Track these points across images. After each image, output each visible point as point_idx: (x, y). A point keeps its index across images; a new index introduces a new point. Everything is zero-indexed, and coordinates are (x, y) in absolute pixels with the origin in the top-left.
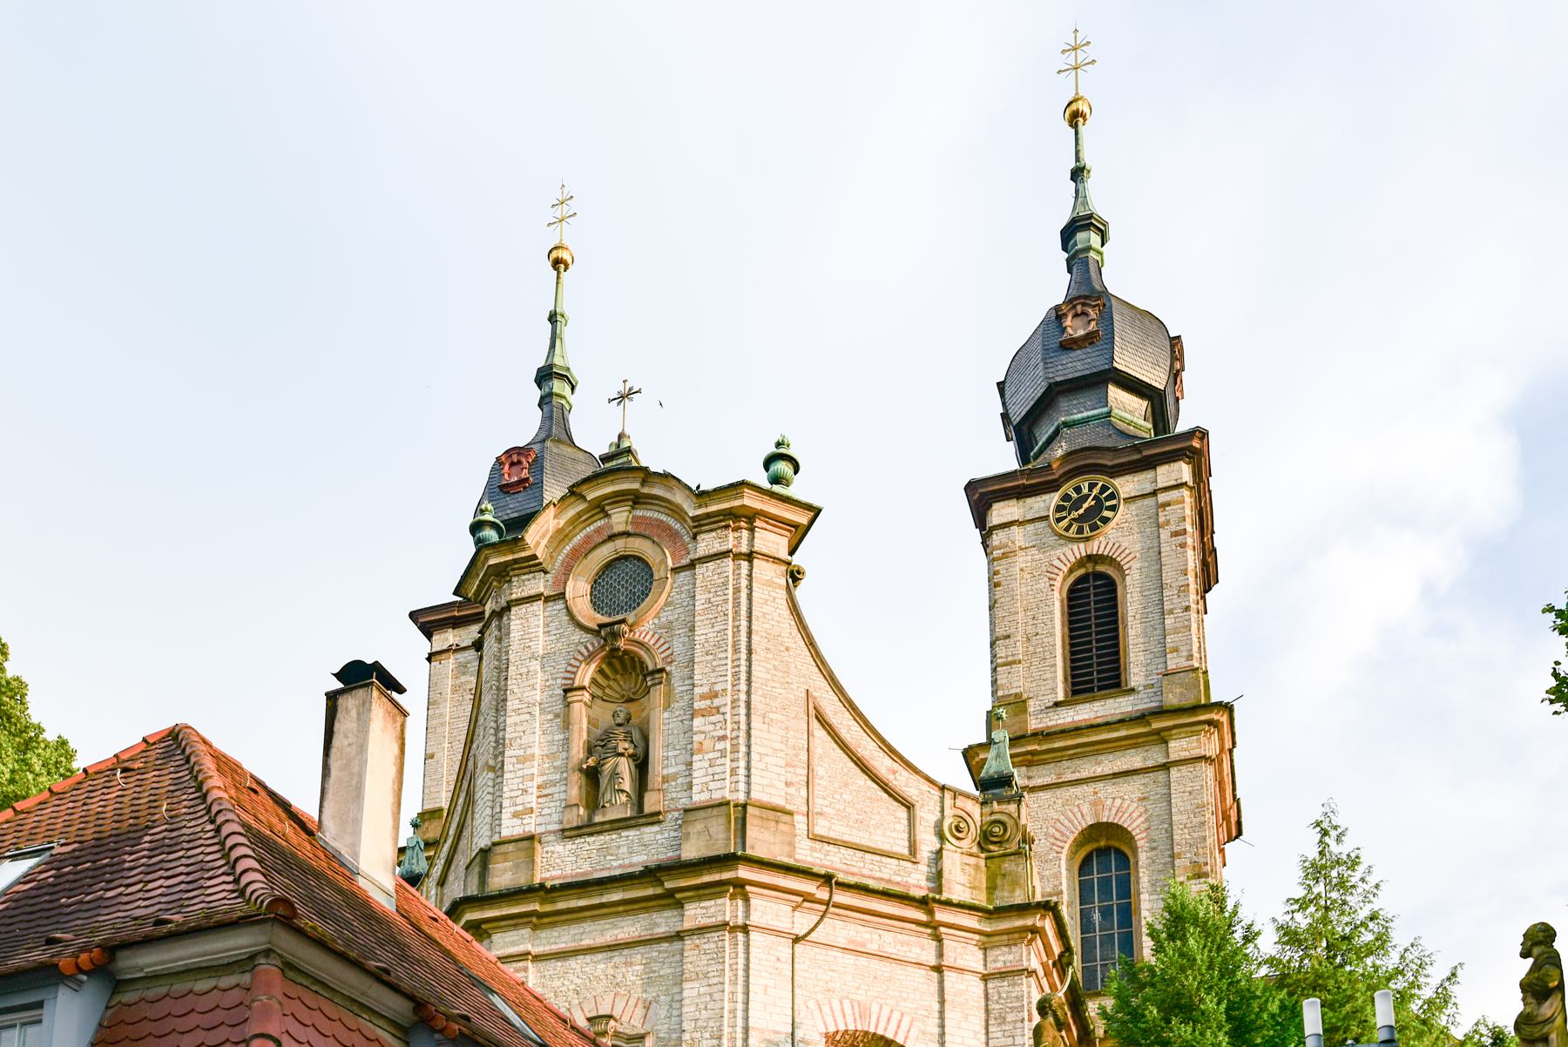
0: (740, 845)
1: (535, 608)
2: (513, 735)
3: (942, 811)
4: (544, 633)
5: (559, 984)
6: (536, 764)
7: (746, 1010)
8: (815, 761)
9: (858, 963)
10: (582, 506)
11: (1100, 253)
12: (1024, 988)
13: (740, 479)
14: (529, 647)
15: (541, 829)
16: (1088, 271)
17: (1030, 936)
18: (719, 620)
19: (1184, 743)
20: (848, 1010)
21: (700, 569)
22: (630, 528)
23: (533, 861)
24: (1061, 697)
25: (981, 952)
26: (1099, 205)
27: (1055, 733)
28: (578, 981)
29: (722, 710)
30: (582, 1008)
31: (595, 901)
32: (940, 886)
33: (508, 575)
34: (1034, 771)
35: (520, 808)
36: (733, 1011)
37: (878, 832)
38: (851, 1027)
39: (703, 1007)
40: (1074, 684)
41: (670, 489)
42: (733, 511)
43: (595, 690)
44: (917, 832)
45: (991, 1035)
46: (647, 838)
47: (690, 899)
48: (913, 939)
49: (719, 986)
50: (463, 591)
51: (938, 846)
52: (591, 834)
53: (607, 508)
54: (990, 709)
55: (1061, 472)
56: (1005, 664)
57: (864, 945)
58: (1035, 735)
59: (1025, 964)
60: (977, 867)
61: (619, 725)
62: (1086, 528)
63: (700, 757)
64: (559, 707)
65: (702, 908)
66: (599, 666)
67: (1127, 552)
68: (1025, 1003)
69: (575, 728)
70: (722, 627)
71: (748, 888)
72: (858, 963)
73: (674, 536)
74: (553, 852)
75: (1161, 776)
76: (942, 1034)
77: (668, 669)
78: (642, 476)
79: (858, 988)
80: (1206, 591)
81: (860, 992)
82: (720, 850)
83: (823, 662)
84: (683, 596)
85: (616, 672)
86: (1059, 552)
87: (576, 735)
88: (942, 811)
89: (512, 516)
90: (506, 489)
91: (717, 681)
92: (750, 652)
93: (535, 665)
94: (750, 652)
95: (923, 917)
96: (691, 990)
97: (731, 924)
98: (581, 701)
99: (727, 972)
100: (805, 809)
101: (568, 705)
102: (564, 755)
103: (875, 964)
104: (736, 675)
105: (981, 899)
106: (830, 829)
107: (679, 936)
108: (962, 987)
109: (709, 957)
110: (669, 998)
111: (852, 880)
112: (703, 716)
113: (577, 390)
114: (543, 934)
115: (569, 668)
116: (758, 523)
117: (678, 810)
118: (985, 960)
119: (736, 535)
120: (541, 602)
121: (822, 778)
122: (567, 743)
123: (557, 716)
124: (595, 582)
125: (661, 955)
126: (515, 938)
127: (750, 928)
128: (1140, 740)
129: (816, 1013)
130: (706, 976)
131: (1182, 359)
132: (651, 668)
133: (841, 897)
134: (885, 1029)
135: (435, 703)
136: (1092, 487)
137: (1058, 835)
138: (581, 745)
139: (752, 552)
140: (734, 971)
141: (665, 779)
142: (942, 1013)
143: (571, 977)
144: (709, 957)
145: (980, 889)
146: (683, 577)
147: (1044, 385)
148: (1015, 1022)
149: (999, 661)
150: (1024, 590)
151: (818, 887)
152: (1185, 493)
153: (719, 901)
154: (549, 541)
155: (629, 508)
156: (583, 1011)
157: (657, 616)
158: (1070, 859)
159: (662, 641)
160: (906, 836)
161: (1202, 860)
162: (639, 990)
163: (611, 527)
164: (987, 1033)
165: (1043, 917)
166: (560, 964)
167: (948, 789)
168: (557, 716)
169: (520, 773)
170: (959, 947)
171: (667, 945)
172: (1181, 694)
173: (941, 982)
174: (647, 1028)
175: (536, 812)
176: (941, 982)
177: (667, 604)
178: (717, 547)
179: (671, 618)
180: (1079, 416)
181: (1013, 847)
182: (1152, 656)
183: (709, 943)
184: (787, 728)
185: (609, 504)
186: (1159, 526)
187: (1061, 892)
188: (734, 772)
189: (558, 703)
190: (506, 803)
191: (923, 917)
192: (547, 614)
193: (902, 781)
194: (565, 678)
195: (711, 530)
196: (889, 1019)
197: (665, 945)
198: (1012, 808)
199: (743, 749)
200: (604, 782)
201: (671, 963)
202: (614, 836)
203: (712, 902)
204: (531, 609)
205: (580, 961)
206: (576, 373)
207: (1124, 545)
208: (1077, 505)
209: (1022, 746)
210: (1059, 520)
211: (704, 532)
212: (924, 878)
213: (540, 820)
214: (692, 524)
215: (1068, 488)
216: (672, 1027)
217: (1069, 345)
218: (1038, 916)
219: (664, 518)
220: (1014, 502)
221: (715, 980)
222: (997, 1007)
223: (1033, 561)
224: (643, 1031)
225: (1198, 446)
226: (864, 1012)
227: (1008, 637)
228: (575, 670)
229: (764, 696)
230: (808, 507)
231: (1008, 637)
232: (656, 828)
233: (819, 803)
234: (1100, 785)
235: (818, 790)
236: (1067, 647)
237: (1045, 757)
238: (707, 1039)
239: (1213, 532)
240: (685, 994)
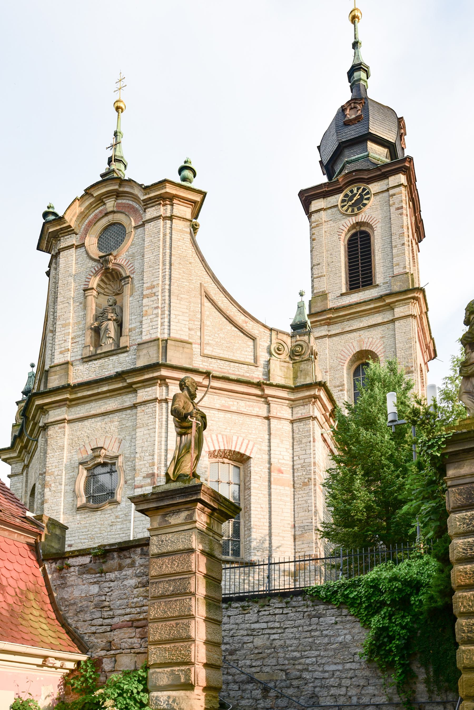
0: (164, 360)
1: (71, 252)
2: (60, 314)
3: (271, 341)
6: (71, 327)
7: (167, 441)
8: (205, 318)
9: (226, 416)
10: (92, 200)
11: (366, 82)
12: (311, 426)
13: (163, 179)
15: (73, 359)
16: (360, 90)
17: (313, 400)
19: (401, 309)
20: (220, 439)
21: (147, 226)
22: (115, 209)
23: (68, 374)
24: (344, 291)
25: (290, 409)
26: (365, 59)
27: (340, 308)
28: (89, 432)
29: (156, 294)
31: (95, 391)
32: (269, 377)
33: (59, 237)
34: (331, 327)
35: (63, 349)
36: (160, 442)
37: (238, 352)
38: (222, 448)
40: (350, 285)
41: (132, 187)
42: (162, 195)
43: (99, 290)
44: (258, 352)
45: (295, 450)
46: (121, 359)
47: (140, 388)
48: (255, 404)
49: (153, 430)
51: (269, 358)
52: (96, 360)
53: (104, 200)
54: (311, 299)
55: (343, 183)
56: (317, 278)
57: (229, 407)
58: (330, 309)
59: (311, 414)
60: (288, 368)
61: (110, 306)
62: (356, 209)
63: (146, 318)
64: (82, 299)
66: (101, 278)
67: (375, 219)
68: (311, 433)
69: (89, 308)
71: (167, 380)
72: (226, 416)
73: (135, 211)
74: (78, 370)
75: (391, 326)
76: (270, 450)
77: (132, 276)
79: (226, 429)
80: (420, 242)
81: (227, 430)
82: (154, 361)
83: (209, 269)
84: (140, 240)
86: (343, 222)
87: (89, 312)
88: (271, 341)
92: (171, 265)
93: (71, 280)
94: (171, 265)
95: (259, 392)
96: (140, 433)
97: (159, 399)
98: (92, 295)
99: (157, 423)
100: (199, 341)
101: (85, 297)
102: (84, 322)
103: (235, 417)
104: (164, 276)
105: (291, 383)
106: (212, 351)
107: (135, 406)
108: (280, 427)
109: (148, 415)
110: (130, 437)
111: (221, 375)
113: (128, 167)
114: (73, 410)
115: (87, 280)
116: (175, 201)
118: (292, 413)
119: (165, 208)
121: (208, 326)
124: (100, 237)
126: (59, 412)
128: (381, 309)
131: (404, 127)
132: (124, 276)
133: (215, 384)
134: (240, 449)
136: (358, 189)
137: (342, 357)
138: (92, 316)
139: (172, 216)
140: (161, 422)
141: (130, 330)
142: (269, 440)
143: (85, 429)
145: (289, 378)
146: (140, 230)
147: (337, 143)
148: (306, 443)
149: (315, 276)
150: (326, 241)
151: (203, 379)
152: (402, 189)
153: (154, 388)
154: (77, 218)
157: (127, 251)
158: (349, 369)
159: (130, 263)
160: (252, 354)
161: (410, 365)
162: (117, 434)
163: (106, 209)
164: (293, 449)
165: (319, 390)
167: (274, 330)
168: (81, 303)
169: (63, 332)
170: (279, 407)
172: (400, 285)
173: (269, 425)
174: (120, 452)
175: (71, 351)
176: (269, 425)
178: (155, 214)
179: (134, 251)
180: (354, 157)
181: (306, 357)
182: (387, 268)
183: (148, 409)
184: (190, 302)
187: (344, 385)
188: (162, 324)
190: (57, 347)
191: (259, 392)
193: (250, 326)
195: (153, 206)
196: (242, 443)
197: (129, 411)
198: (306, 338)
199: (167, 312)
200: (102, 333)
202: (106, 360)
203: (150, 389)
206: (126, 159)
207: (373, 216)
208: (351, 199)
209: (325, 315)
210: (343, 207)
212: (261, 374)
213: (73, 354)
214: (143, 204)
215: (347, 191)
217: (347, 123)
218: (317, 390)
219: (131, 203)
220: (322, 199)
221: (151, 427)
222: (298, 436)
223: (331, 227)
224: (118, 454)
225: (408, 165)
227: (319, 264)
229: (178, 286)
230: (200, 192)
231: (319, 264)
232: (125, 354)
233: (207, 338)
234: (362, 332)
235: (206, 332)
236: (347, 267)
237: (336, 320)
239: (420, 211)
240: (137, 435)
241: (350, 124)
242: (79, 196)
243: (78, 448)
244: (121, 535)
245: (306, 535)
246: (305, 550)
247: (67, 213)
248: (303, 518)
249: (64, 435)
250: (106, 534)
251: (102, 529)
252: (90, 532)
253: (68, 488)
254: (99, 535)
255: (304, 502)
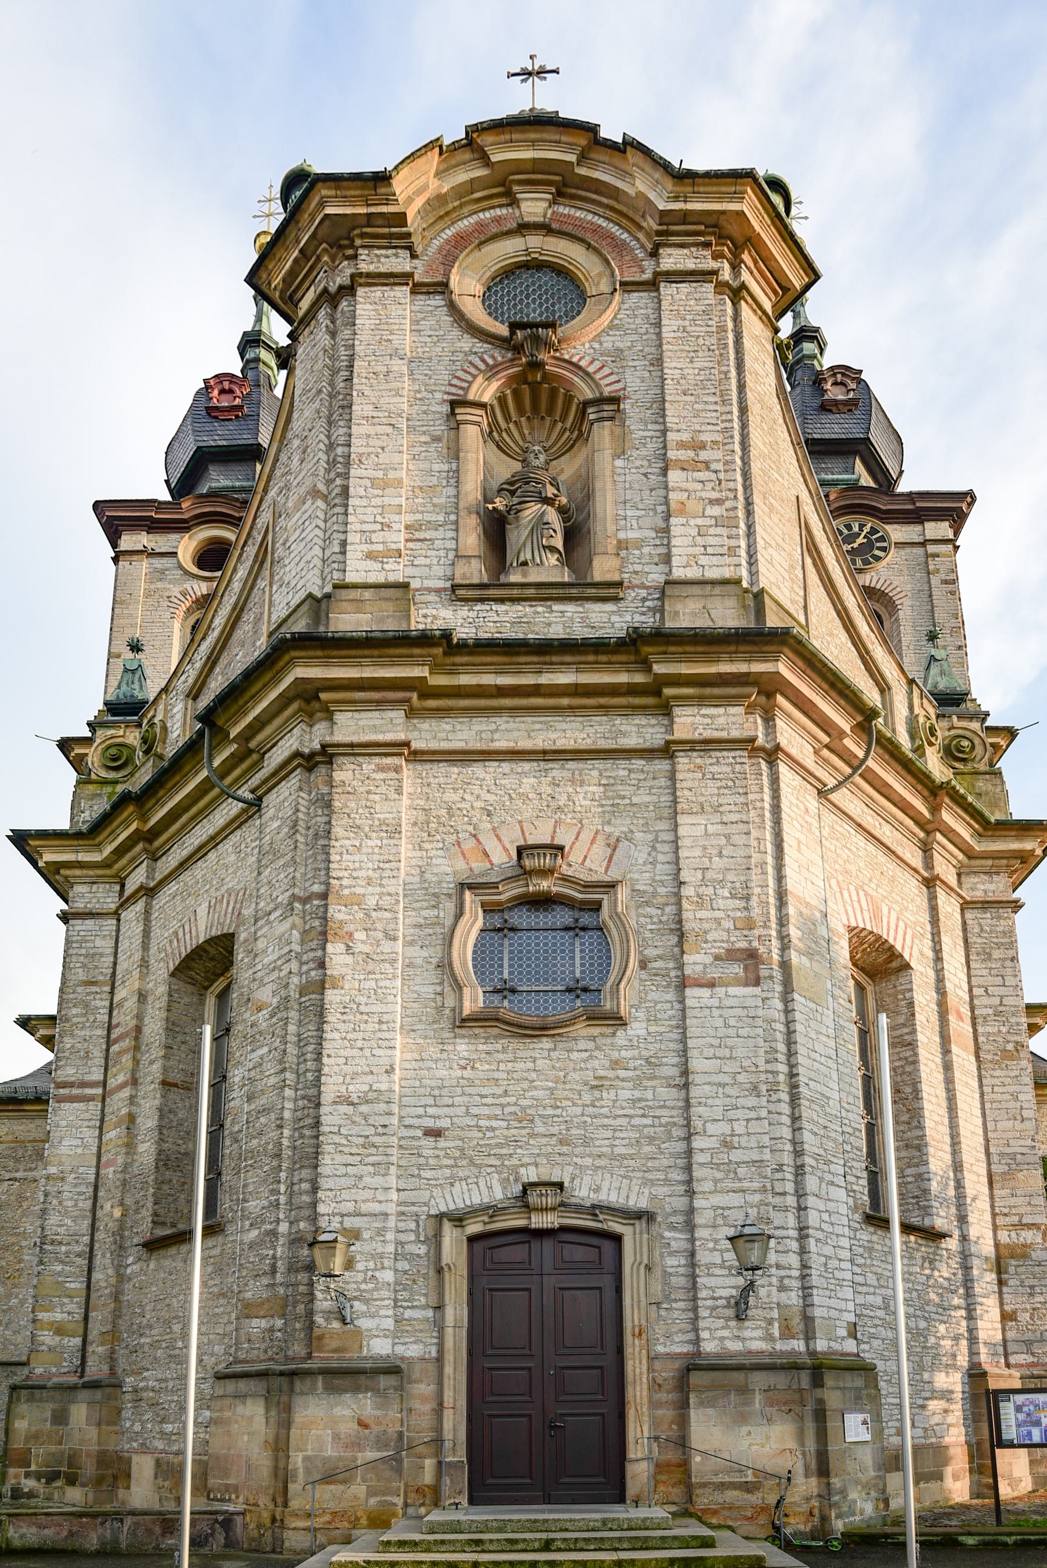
4: (411, 331)
5: (456, 797)
10: (481, 172)
14: (388, 340)
18: (700, 354)
28: (491, 798)
30: (497, 836)
33: (352, 246)
39: (715, 852)
47: (685, 700)
50: (264, 276)
52: (501, 600)
63: (683, 520)
64: (440, 428)
65: (703, 716)
70: (706, 364)
78: (583, 142)
84: (638, 321)
85: (521, 411)
89: (220, 443)
90: (212, 413)
91: (703, 428)
109: (719, 784)
110: (650, 837)
112: (683, 469)
117: (643, 586)
120: (407, 289)
122: (456, 477)
123: (437, 439)
125: (632, 776)
126: (378, 722)
127: (781, 755)
129: (838, 895)
130: (717, 809)
135: (122, 602)
136: (861, 527)
143: (476, 790)
144: (719, 784)
148: (1004, 960)
155: (550, 197)
156: (499, 839)
157: (597, 338)
166: (456, 770)
171: (643, 762)
177: (611, 326)
179: (620, 345)
185: (520, 183)
186: (929, 573)
189: (438, 423)
192: (414, 308)
194: (448, 393)
195: (682, 246)
197: (639, 763)
201: (651, 788)
202: (540, 609)
204: (392, 294)
205: (491, 770)
211: (671, 245)
216: (658, 878)
222: (979, 940)
226: (876, 915)
228: (465, 385)
232: (609, 607)
238: (723, 898)
241: (834, 409)
242: (447, 141)
243: (452, 838)
244: (636, 1121)
245: (1020, 1175)
246: (1022, 1210)
247: (405, 172)
248: (1010, 1135)
249: (400, 793)
250: (579, 1110)
251: (559, 1093)
252: (512, 1100)
253: (418, 954)
254: (550, 1111)
255: (1008, 1097)
